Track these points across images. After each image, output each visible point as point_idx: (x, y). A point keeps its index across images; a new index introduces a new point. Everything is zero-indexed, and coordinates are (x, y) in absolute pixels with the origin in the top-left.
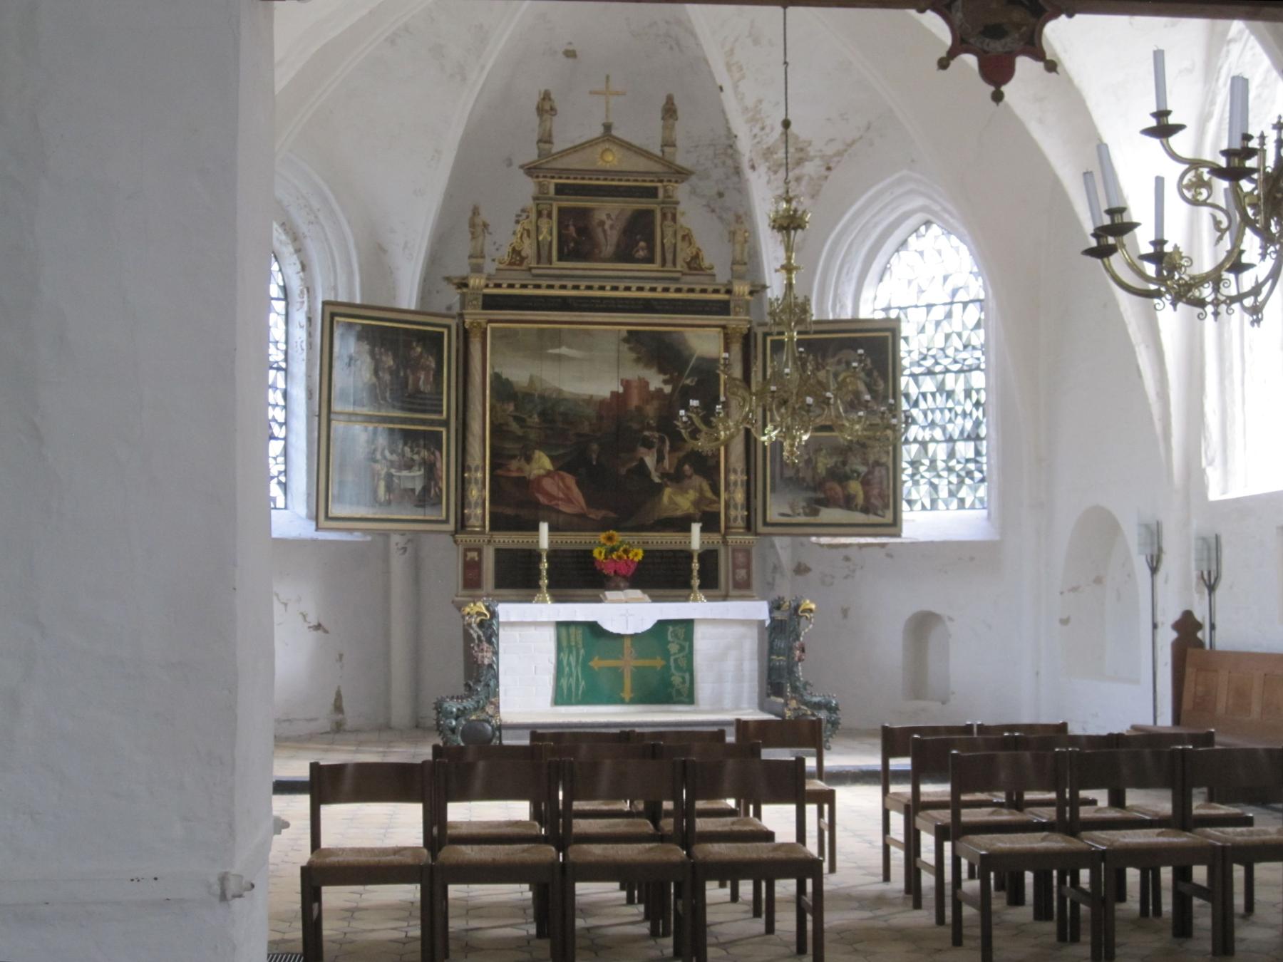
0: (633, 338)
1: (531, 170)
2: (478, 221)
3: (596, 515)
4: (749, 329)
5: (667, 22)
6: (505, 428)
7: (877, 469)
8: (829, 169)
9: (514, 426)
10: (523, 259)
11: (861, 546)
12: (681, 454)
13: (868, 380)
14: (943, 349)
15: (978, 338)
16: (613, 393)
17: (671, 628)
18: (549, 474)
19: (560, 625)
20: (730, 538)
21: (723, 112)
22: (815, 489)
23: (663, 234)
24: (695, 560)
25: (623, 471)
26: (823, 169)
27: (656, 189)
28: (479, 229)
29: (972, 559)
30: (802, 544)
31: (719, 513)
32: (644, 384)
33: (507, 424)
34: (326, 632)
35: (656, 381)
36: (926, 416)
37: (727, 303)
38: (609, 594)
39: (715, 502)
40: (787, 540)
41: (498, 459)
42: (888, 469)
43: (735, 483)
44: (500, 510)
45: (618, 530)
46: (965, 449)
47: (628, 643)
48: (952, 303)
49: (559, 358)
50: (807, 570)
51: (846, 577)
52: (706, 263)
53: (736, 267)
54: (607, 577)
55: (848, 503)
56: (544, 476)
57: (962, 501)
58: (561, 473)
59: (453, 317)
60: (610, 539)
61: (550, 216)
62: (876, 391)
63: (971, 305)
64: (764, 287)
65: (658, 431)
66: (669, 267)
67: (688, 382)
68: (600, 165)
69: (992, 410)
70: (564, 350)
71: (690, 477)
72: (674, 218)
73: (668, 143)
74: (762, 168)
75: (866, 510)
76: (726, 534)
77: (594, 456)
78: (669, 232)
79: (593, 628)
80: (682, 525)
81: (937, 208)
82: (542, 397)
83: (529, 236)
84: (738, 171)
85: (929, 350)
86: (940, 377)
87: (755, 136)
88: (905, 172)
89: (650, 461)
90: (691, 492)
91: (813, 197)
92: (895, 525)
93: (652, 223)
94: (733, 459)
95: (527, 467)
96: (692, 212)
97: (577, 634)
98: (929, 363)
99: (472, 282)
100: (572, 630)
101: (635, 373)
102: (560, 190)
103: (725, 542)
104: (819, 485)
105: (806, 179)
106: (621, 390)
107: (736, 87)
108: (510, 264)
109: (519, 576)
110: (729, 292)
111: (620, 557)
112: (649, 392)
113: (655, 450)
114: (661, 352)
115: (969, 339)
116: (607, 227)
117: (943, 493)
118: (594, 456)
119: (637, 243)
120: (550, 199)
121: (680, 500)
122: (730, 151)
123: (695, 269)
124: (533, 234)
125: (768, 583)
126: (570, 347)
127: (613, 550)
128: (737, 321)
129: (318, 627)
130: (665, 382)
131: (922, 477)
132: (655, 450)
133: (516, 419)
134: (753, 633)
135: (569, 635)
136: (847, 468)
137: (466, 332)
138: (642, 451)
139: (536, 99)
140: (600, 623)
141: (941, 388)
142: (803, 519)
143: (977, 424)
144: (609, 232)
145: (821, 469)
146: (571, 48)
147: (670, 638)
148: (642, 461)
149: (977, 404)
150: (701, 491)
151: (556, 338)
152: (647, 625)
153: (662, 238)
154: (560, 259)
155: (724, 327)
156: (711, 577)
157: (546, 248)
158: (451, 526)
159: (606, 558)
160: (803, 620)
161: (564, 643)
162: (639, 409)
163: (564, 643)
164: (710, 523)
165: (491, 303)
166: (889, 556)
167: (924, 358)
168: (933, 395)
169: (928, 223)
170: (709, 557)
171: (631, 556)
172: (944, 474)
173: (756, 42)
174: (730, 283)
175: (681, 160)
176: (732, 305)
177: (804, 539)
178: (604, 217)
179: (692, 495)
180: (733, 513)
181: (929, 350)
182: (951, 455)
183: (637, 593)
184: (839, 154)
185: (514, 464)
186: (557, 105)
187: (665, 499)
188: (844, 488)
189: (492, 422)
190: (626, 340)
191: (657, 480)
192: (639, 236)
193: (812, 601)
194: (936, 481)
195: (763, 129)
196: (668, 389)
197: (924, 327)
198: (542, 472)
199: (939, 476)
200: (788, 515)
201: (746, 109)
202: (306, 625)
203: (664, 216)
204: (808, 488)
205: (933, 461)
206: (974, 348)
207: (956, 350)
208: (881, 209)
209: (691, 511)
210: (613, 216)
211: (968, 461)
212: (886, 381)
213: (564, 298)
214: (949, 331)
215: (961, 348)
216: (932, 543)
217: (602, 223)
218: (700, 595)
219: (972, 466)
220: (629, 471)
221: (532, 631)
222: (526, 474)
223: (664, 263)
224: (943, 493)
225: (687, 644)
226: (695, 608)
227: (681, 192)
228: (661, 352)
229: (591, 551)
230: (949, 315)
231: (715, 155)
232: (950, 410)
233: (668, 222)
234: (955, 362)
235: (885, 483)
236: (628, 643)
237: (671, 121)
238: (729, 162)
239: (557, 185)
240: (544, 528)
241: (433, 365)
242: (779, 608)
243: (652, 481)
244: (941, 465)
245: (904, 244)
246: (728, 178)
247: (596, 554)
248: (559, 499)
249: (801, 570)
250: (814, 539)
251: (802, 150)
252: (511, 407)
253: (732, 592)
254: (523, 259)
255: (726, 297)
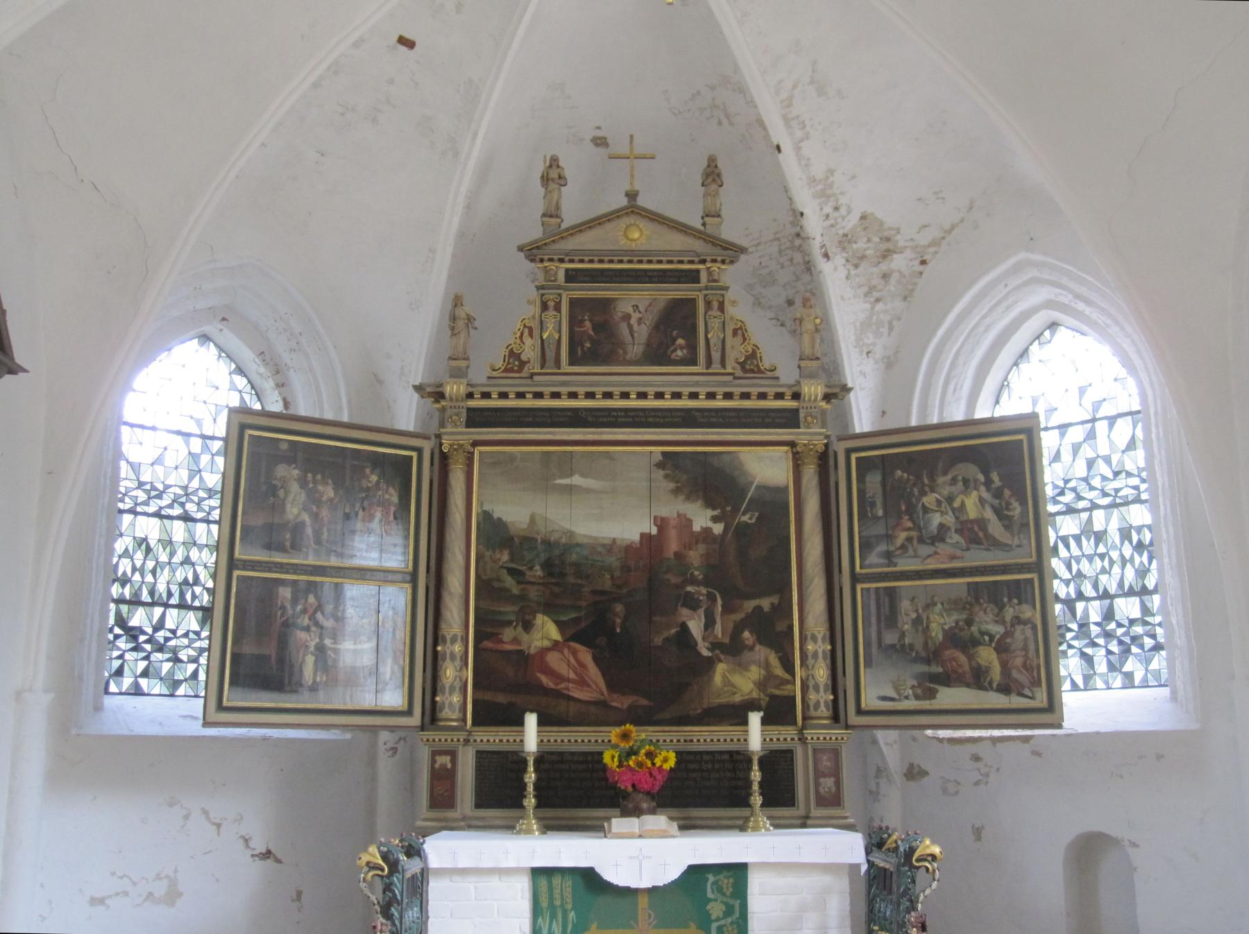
0: (670, 462)
1: (532, 251)
2: (461, 313)
3: (621, 702)
4: (826, 445)
5: (713, 88)
6: (496, 584)
7: (1019, 628)
8: (923, 262)
9: (509, 582)
10: (523, 364)
11: (995, 740)
12: (739, 616)
13: (996, 502)
14: (1086, 480)
15: (1137, 460)
16: (642, 535)
17: (711, 878)
18: (556, 646)
19: (537, 872)
20: (808, 733)
21: (786, 190)
22: (928, 662)
23: (708, 328)
24: (756, 767)
25: (658, 641)
26: (917, 262)
27: (698, 271)
28: (461, 324)
29: (1160, 757)
30: (914, 739)
31: (794, 698)
32: (686, 522)
33: (499, 580)
34: (279, 861)
35: (701, 518)
36: (1069, 568)
37: (796, 411)
38: (619, 824)
39: (788, 682)
40: (893, 735)
41: (487, 626)
42: (1034, 628)
43: (815, 655)
44: (488, 696)
45: (637, 723)
46: (1128, 608)
47: (643, 901)
48: (1094, 420)
49: (570, 489)
50: (924, 773)
51: (977, 783)
52: (766, 364)
53: (803, 364)
54: (625, 795)
55: (978, 679)
56: (548, 649)
57: (1129, 676)
58: (572, 644)
59: (426, 438)
60: (625, 736)
61: (558, 308)
62: (1009, 518)
63: (1119, 421)
64: (846, 389)
65: (706, 586)
66: (716, 367)
67: (745, 518)
68: (623, 244)
69: (1165, 549)
70: (577, 480)
71: (752, 648)
72: (721, 308)
73: (712, 214)
74: (839, 260)
75: (1005, 689)
76: (804, 727)
77: (618, 621)
78: (715, 324)
79: (589, 879)
80: (737, 714)
81: (1065, 298)
82: (547, 543)
83: (531, 335)
84: (809, 267)
85: (1066, 481)
86: (1085, 516)
87: (827, 216)
88: (1022, 255)
89: (696, 627)
90: (754, 668)
91: (905, 298)
92: (1052, 707)
93: (694, 315)
94: (810, 621)
95: (525, 637)
96: (745, 305)
97: (566, 885)
98: (1069, 497)
99: (448, 390)
100: (557, 880)
101: (672, 508)
102: (571, 276)
103: (802, 740)
104: (933, 655)
105: (895, 276)
106: (654, 531)
107: (798, 149)
108: (506, 370)
109: (500, 792)
110: (796, 396)
111: (640, 764)
112: (692, 533)
113: (701, 612)
114: (709, 481)
115: (1121, 462)
116: (633, 321)
117: (1101, 667)
118: (618, 621)
119: (674, 340)
120: (559, 287)
121: (736, 680)
122: (798, 242)
123: (752, 371)
124: (536, 332)
125: (871, 792)
126: (583, 475)
127: (632, 752)
128: (810, 435)
129: (268, 854)
130: (715, 519)
131: (1070, 646)
132: (701, 612)
133: (511, 572)
134: (844, 884)
135: (551, 889)
136: (974, 629)
137: (444, 457)
138: (685, 612)
139: (540, 168)
140: (597, 870)
141: (1087, 530)
142: (912, 704)
143: (1142, 573)
144: (636, 327)
145: (937, 633)
146: (599, 134)
147: (710, 895)
148: (684, 628)
149: (1140, 547)
150: (767, 666)
151: (567, 465)
152: (672, 873)
153: (706, 333)
154: (572, 362)
155: (792, 444)
156: (778, 790)
157: (553, 347)
158: (416, 720)
159: (620, 766)
160: (921, 875)
161: (544, 904)
162: (678, 555)
163: (544, 904)
164: (779, 712)
165: (476, 418)
166: (1036, 753)
167: (1062, 493)
168: (1077, 539)
169: (1053, 326)
170: (778, 766)
171: (658, 761)
172: (1101, 641)
173: (821, 92)
174: (798, 383)
175: (728, 233)
176: (802, 415)
177: (915, 733)
178: (630, 310)
179: (755, 673)
180: (812, 696)
181: (1066, 481)
182: (1109, 615)
183: (660, 821)
184: (935, 243)
185: (508, 634)
186: (568, 173)
187: (718, 679)
188: (971, 658)
189: (478, 576)
190: (660, 465)
191: (705, 653)
192: (676, 332)
193: (934, 842)
194: (1089, 651)
195: (836, 209)
196: (718, 529)
197: (1058, 452)
198: (546, 643)
199: (1094, 645)
200: (892, 699)
201: (813, 181)
202: (250, 852)
203: (708, 304)
204: (918, 659)
205: (1084, 626)
206: (1129, 474)
207: (1104, 478)
208: (991, 310)
209: (755, 695)
210: (642, 309)
211: (1132, 622)
212: (1023, 503)
213: (575, 411)
214: (1091, 455)
215: (1110, 476)
216: (1098, 733)
217: (627, 317)
218: (763, 820)
219: (1138, 629)
220: (667, 640)
221: (495, 882)
222: (524, 647)
223: (709, 363)
224: (1101, 667)
225: (737, 903)
226: (755, 846)
227: (733, 276)
228: (709, 481)
229: (601, 754)
230: (1091, 435)
231: (780, 252)
232: (1102, 557)
233: (715, 312)
234: (1105, 494)
235: (1032, 647)
236: (643, 901)
237: (714, 186)
238: (798, 258)
239: (567, 270)
240: (531, 720)
241: (395, 499)
242: (880, 845)
243: (699, 654)
244: (1094, 630)
245: (1024, 354)
246: (798, 279)
247: (607, 758)
248: (568, 680)
249: (914, 773)
250: (929, 732)
251: (888, 239)
252: (505, 557)
253: (815, 812)
254: (523, 364)
255: (792, 404)
